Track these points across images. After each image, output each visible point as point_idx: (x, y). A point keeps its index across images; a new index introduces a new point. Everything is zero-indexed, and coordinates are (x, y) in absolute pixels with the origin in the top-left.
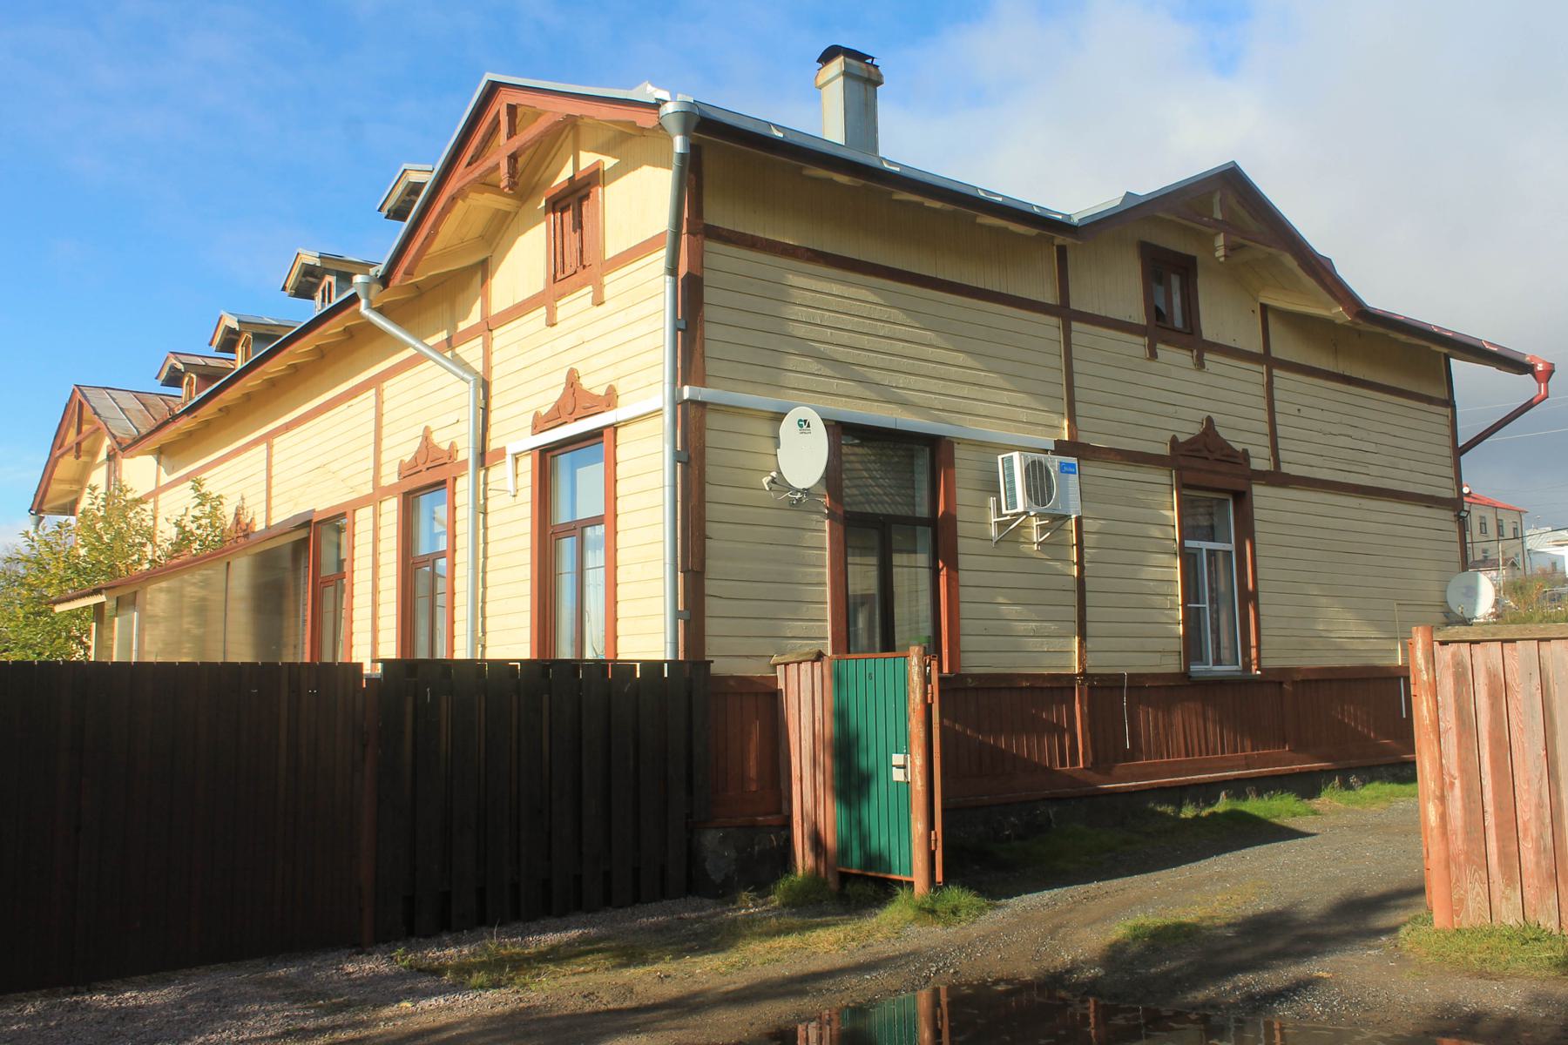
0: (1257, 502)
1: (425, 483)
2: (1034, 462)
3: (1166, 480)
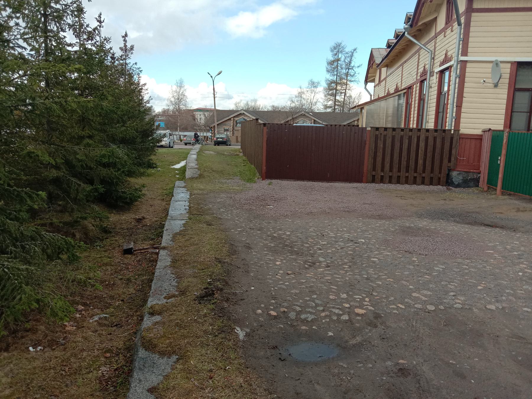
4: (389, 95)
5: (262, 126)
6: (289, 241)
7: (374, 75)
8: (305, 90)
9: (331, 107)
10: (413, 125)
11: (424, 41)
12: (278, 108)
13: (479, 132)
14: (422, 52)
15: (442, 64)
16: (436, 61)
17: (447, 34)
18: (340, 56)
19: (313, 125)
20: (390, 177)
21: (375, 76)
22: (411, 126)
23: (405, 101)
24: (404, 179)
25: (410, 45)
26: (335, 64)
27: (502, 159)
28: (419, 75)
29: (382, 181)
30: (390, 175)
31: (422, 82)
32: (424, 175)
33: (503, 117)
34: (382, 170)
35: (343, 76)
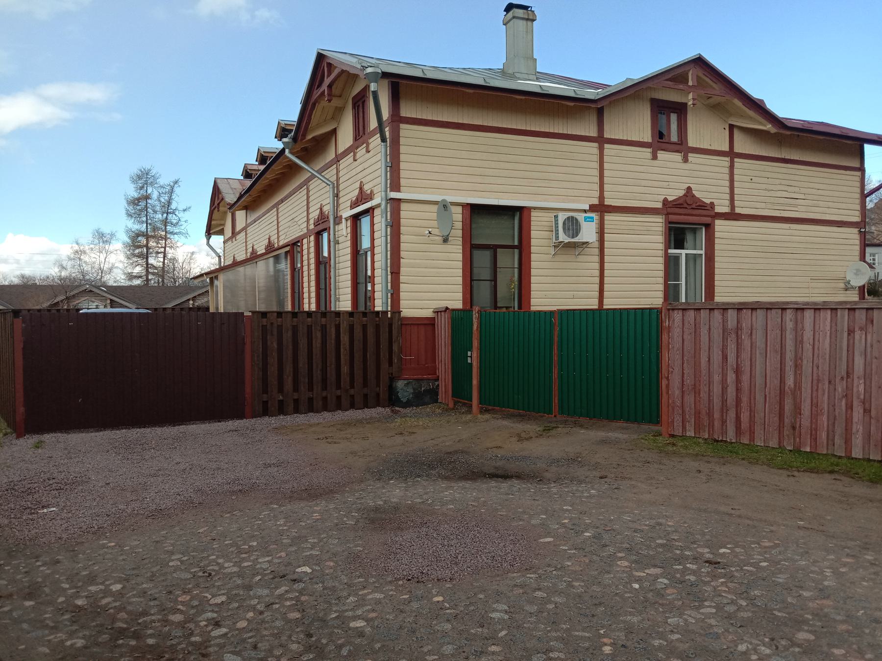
0: (717, 228)
1: (321, 227)
2: (568, 218)
3: (660, 220)
4: (254, 257)
5: (10, 317)
6: (123, 615)
7: (222, 222)
8: (87, 247)
9: (141, 277)
10: (309, 304)
11: (320, 164)
12: (34, 278)
13: (428, 313)
14: (313, 184)
15: (354, 205)
16: (341, 201)
17: (358, 155)
18: (149, 191)
19: (109, 310)
20: (296, 401)
21: (224, 225)
22: (306, 308)
23: (289, 266)
24: (321, 403)
25: (292, 170)
26: (143, 204)
27: (475, 355)
28: (312, 222)
29: (282, 410)
30: (296, 397)
31: (318, 235)
32: (352, 392)
33: (460, 288)
34: (281, 390)
35: (159, 225)
